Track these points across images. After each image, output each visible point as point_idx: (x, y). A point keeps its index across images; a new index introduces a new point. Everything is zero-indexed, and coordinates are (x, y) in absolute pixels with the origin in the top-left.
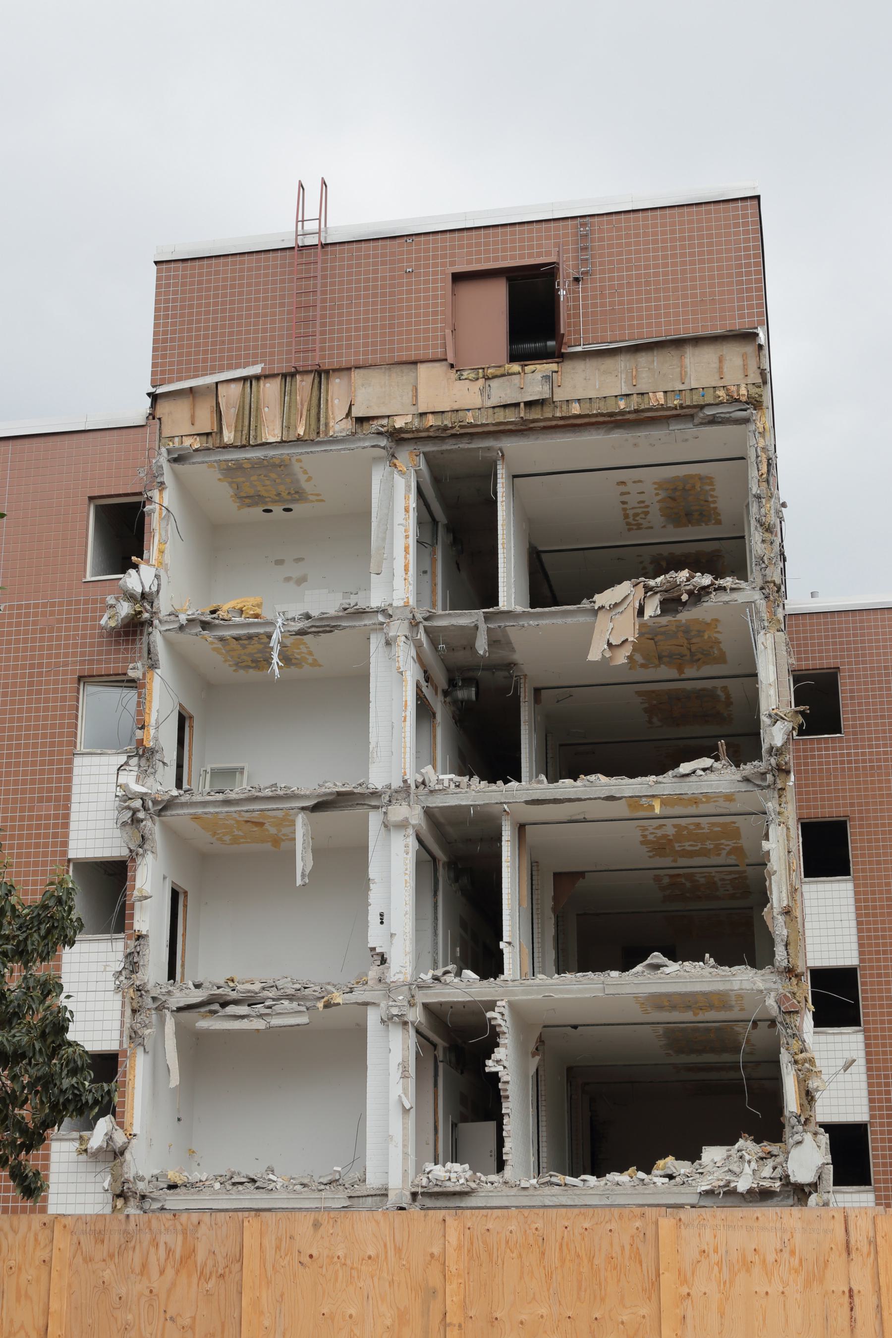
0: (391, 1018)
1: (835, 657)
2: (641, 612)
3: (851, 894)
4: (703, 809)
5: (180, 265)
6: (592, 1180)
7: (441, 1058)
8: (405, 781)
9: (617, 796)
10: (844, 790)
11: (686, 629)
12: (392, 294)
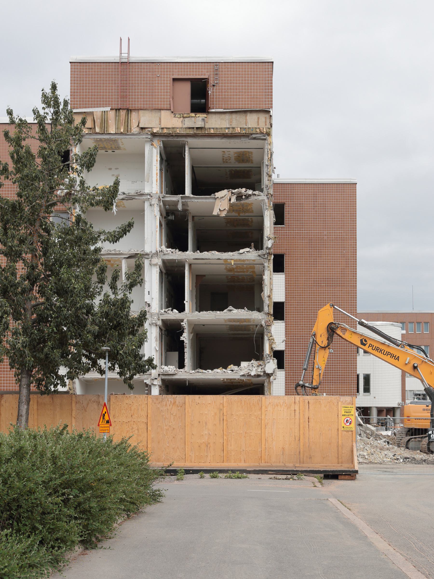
0: (153, 324)
1: (284, 199)
2: (230, 200)
3: (284, 279)
4: (245, 263)
5: (79, 64)
6: (210, 371)
7: (163, 333)
8: (157, 251)
10: (284, 245)
11: (243, 205)
12: (152, 84)
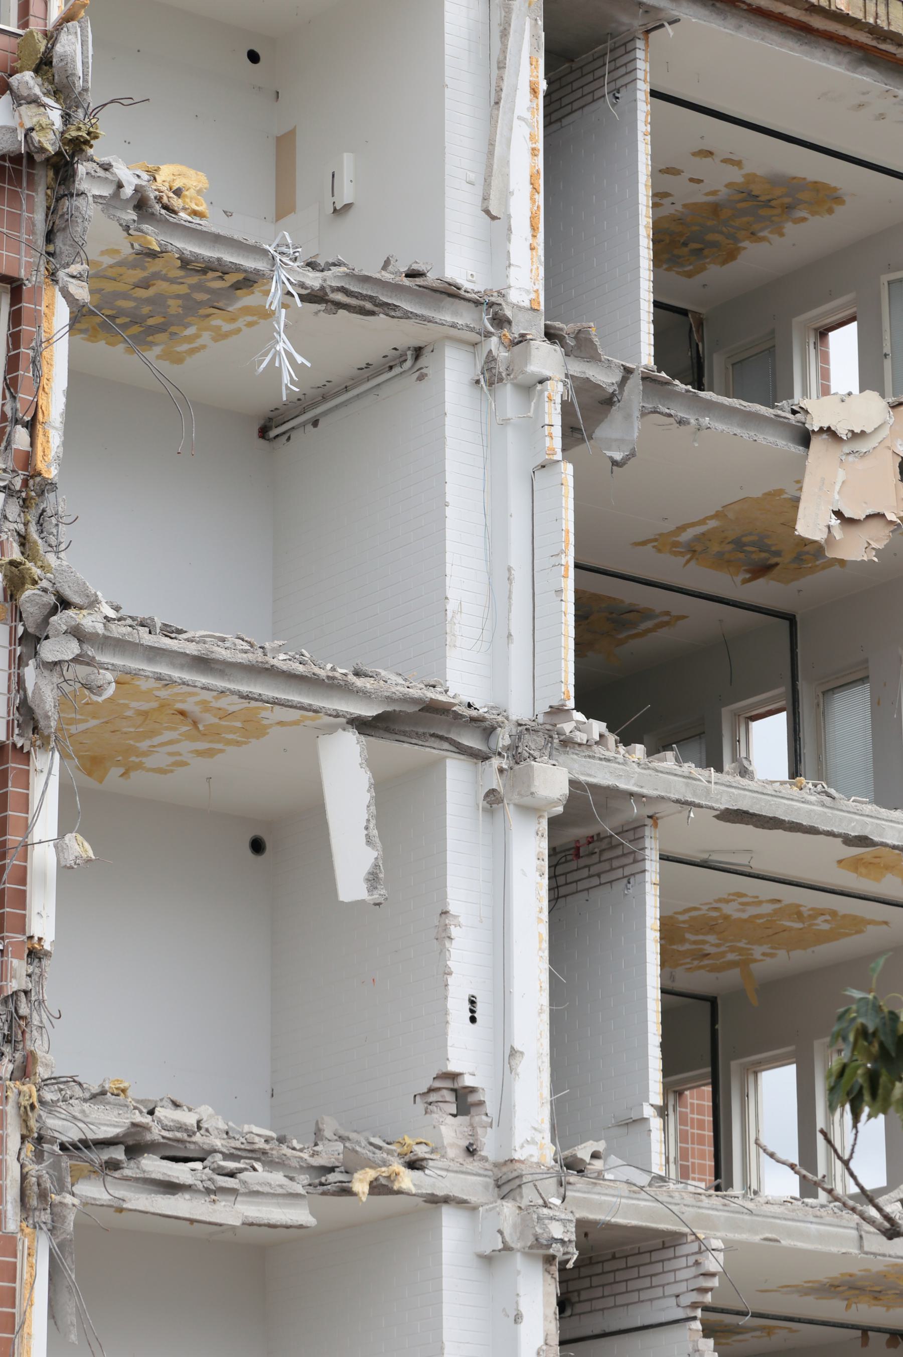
9: (876, 839)
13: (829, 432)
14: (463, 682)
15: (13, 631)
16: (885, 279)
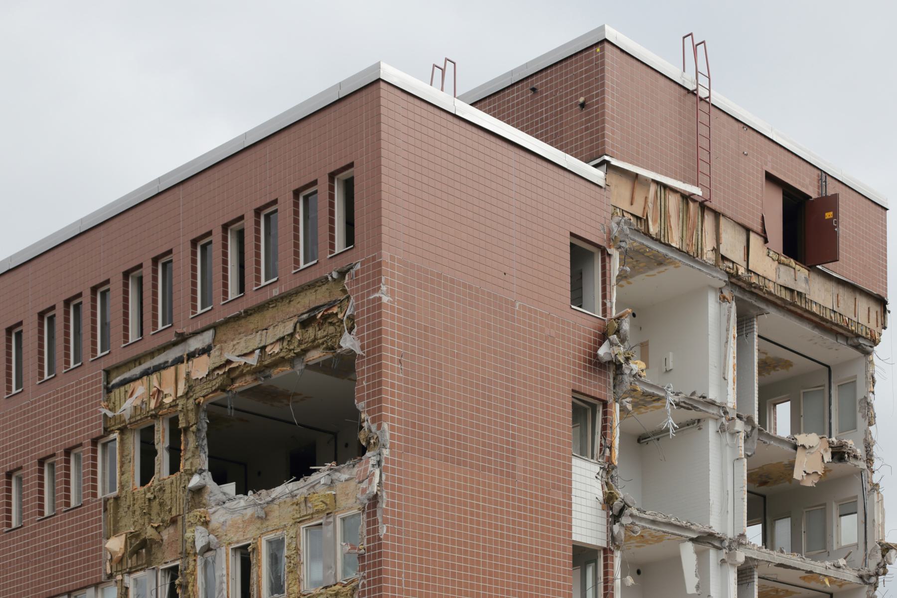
13: (803, 446)
14: (716, 527)
15: (608, 513)
16: (802, 391)
